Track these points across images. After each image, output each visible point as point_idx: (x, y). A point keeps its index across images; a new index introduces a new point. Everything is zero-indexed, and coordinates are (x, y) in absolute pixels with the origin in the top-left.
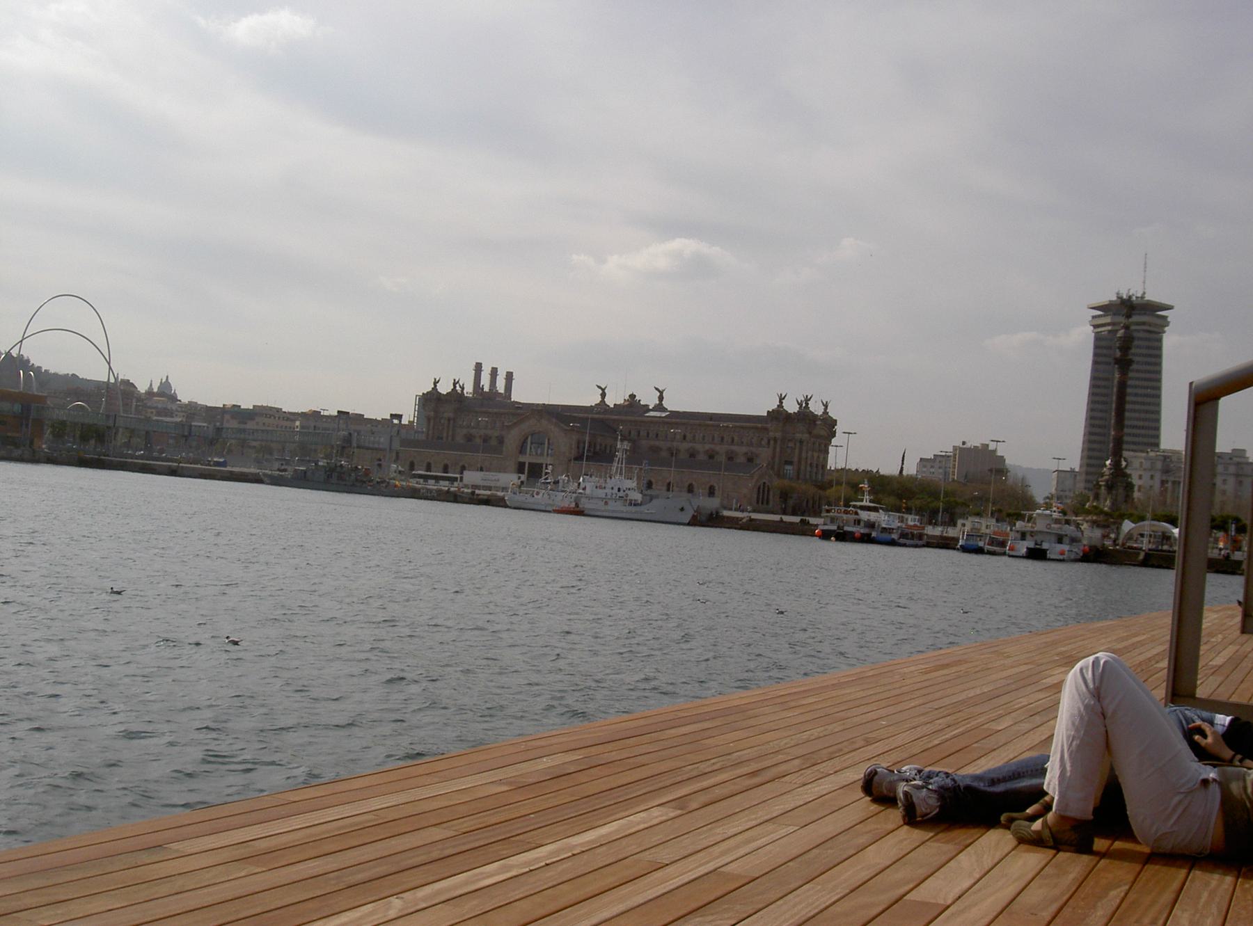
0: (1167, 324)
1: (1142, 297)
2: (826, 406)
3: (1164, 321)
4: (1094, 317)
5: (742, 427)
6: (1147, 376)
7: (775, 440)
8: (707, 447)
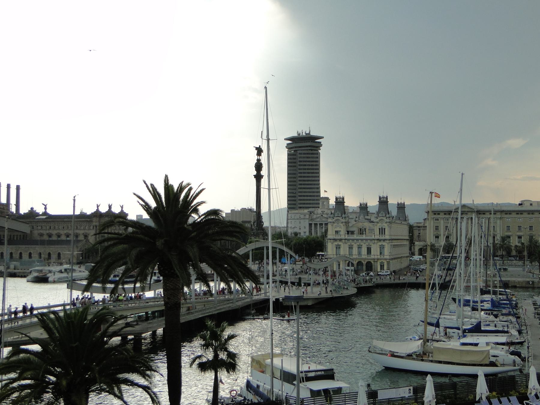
0: (321, 145)
1: (309, 134)
2: (122, 207)
3: (320, 145)
4: (191, 189)
5: (80, 221)
6: (312, 171)
7: (96, 226)
8: (65, 232)
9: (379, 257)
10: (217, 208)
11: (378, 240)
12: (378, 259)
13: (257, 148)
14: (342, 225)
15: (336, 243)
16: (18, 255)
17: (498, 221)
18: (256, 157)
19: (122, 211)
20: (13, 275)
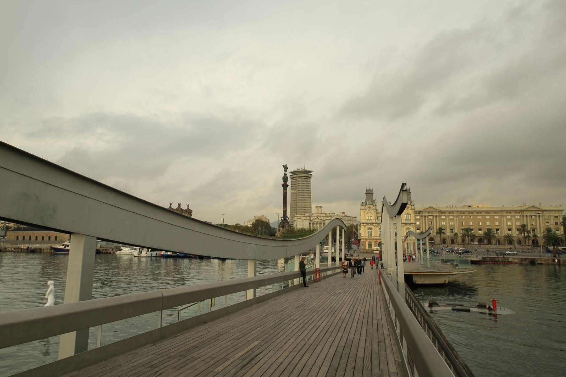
2: (188, 206)
9: (367, 237)
10: (307, 169)
11: (405, 224)
12: (366, 239)
13: (284, 166)
14: (372, 211)
15: (407, 227)
16: (48, 238)
17: (455, 218)
18: (284, 172)
19: (188, 208)
20: (261, 229)
